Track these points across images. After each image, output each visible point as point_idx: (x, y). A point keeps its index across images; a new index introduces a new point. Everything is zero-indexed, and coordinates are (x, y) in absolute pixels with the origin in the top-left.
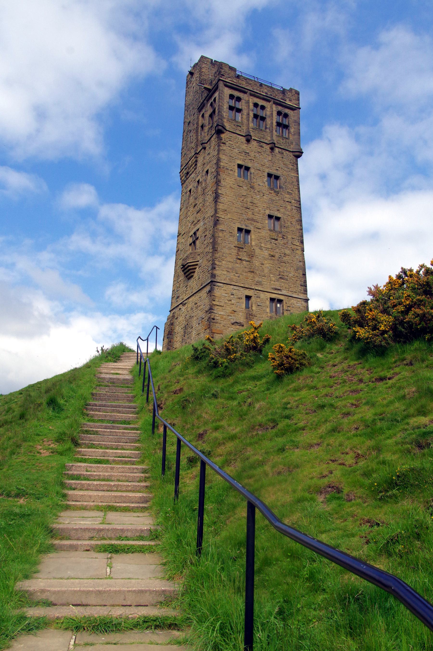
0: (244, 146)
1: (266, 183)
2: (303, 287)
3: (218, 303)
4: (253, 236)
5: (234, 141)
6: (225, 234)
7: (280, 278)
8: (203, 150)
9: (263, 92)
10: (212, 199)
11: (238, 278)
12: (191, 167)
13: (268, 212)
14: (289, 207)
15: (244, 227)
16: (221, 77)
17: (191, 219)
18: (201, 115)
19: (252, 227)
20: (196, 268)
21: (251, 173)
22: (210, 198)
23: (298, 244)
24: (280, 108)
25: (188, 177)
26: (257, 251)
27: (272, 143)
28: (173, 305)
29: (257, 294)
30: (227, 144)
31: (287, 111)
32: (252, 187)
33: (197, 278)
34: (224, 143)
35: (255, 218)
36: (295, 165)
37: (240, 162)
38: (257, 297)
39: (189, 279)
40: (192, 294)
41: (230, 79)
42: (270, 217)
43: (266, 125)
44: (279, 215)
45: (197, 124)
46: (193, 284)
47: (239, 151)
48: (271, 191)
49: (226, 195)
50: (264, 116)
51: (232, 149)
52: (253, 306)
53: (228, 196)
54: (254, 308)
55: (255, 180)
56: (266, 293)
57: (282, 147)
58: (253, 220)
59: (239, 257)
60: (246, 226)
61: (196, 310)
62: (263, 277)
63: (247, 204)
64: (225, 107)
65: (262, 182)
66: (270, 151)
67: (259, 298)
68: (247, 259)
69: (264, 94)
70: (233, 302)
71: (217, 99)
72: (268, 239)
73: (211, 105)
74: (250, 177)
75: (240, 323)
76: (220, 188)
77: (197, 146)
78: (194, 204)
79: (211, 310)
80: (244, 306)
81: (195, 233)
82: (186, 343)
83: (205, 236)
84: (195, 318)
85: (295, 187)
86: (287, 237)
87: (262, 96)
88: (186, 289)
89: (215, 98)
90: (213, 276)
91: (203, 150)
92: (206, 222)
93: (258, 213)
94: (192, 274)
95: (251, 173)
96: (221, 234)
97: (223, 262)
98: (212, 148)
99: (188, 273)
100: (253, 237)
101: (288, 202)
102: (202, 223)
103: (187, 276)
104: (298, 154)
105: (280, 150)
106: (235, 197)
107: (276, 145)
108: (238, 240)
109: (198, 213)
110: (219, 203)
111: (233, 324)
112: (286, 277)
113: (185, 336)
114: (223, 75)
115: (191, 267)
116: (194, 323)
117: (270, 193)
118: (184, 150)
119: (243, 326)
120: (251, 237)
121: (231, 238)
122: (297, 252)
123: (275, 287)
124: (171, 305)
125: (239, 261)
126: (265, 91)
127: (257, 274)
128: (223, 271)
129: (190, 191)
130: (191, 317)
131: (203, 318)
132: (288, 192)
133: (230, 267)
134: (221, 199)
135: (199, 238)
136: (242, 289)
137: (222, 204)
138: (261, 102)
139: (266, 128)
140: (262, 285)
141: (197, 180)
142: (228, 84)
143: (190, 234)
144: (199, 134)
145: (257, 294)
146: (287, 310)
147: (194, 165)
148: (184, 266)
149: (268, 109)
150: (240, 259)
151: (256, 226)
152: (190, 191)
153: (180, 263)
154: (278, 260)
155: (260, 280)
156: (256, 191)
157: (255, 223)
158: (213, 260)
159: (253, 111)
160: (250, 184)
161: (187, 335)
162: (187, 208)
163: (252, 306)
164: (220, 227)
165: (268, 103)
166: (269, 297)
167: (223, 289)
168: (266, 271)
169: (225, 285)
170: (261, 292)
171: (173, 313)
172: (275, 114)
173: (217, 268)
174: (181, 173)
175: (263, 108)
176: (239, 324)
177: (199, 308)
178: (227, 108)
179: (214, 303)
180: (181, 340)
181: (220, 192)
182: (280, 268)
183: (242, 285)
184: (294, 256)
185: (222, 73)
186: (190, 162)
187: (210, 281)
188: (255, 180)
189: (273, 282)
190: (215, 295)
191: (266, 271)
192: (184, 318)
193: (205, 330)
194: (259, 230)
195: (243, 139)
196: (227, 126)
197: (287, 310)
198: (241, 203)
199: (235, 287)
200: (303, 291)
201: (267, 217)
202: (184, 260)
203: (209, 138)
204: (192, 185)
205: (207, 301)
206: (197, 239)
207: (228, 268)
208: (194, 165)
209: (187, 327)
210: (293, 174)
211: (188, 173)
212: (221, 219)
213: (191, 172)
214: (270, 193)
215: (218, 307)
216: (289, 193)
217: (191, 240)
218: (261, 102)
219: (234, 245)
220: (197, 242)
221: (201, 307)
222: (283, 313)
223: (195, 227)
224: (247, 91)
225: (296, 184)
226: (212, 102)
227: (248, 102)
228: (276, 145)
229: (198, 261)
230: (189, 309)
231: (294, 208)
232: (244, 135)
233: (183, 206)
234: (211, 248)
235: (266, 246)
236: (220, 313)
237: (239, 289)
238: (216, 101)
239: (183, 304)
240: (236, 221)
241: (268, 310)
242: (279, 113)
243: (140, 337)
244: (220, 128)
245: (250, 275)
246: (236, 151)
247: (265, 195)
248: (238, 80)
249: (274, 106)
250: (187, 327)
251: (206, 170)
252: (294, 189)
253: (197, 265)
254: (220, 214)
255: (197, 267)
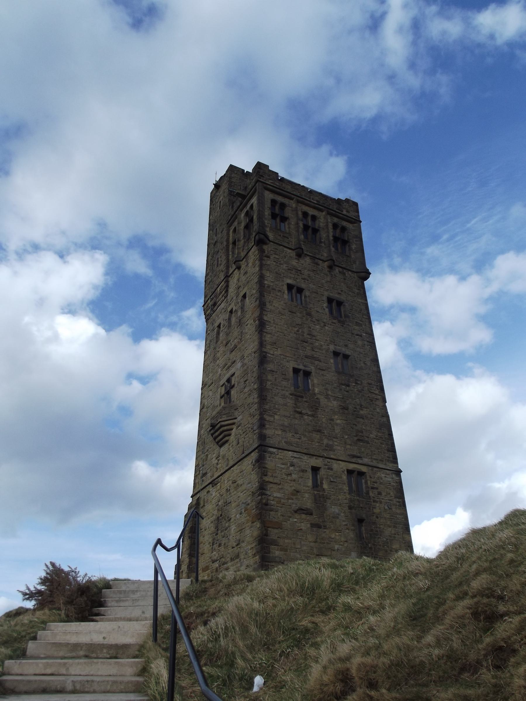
0: (294, 262)
1: (327, 310)
2: (391, 453)
3: (271, 480)
4: (314, 380)
5: (281, 255)
6: (277, 376)
7: (358, 440)
8: (237, 270)
9: (313, 199)
10: (254, 329)
11: (298, 440)
12: (220, 294)
13: (332, 348)
14: (360, 343)
15: (301, 367)
16: (260, 178)
17: (221, 362)
18: (231, 231)
19: (313, 368)
20: (232, 429)
21: (305, 297)
22: (250, 327)
23: (377, 392)
24: (336, 220)
25: (215, 308)
26: (323, 401)
27: (331, 260)
28: (197, 486)
29: (328, 464)
30: (272, 257)
31: (344, 223)
32: (309, 314)
33: (235, 443)
34: (268, 257)
35: (315, 356)
36: (361, 289)
37: (289, 281)
38: (329, 469)
39: (221, 446)
40: (227, 468)
41: (270, 181)
42: (336, 354)
43: (320, 238)
44: (348, 352)
45: (228, 241)
46: (229, 451)
47: (287, 268)
48: (334, 321)
49: (274, 323)
50: (317, 228)
51: (278, 264)
52: (324, 482)
53: (277, 324)
54: (325, 486)
55: (311, 306)
56: (340, 462)
57: (342, 266)
58: (313, 358)
59: (297, 409)
60: (305, 366)
61: (235, 492)
62: (334, 440)
63: (303, 335)
64: (266, 213)
65: (321, 309)
66: (329, 270)
67: (332, 469)
68: (310, 413)
69: (316, 202)
70: (294, 476)
71: (255, 208)
72: (336, 385)
73: (247, 214)
74: (306, 301)
75: (307, 509)
76: (264, 313)
77: (228, 267)
78: (224, 342)
79: (262, 488)
80: (310, 483)
81: (229, 381)
82: (220, 545)
83: (246, 381)
84: (234, 505)
85: (364, 317)
86: (362, 383)
87: (312, 204)
88: (216, 461)
89: (252, 206)
90: (262, 437)
91: (237, 270)
92: (246, 361)
93: (320, 349)
94: (227, 438)
95: (305, 297)
96: (270, 377)
97: (276, 417)
98: (250, 264)
99: (217, 434)
100: (315, 381)
101: (357, 335)
102: (239, 365)
103: (217, 443)
104: (367, 275)
105: (341, 269)
106: (286, 326)
107: (335, 264)
108: (296, 386)
109: (232, 352)
110: (265, 334)
111: (296, 512)
112: (366, 439)
113: (217, 534)
114: (262, 176)
115: (225, 428)
116: (233, 512)
117: (332, 323)
118: (208, 277)
119: (311, 514)
120: (312, 381)
121: (284, 383)
122: (377, 403)
123: (352, 453)
124: (194, 487)
125: (297, 415)
126: (317, 198)
127: (326, 434)
128: (277, 429)
129: (219, 326)
130: (227, 504)
131: (248, 504)
132: (356, 322)
133: (286, 424)
134: (268, 328)
135: (236, 385)
136: (305, 457)
137: (269, 336)
138: (311, 212)
139: (321, 242)
140: (334, 451)
141: (229, 309)
142: (268, 186)
143: (221, 383)
144: (231, 253)
145: (328, 464)
146: (372, 488)
147: (224, 292)
148: (213, 426)
149: (322, 220)
150: (300, 413)
151: (318, 367)
152: (219, 326)
153: (207, 423)
154: (353, 414)
155: (331, 443)
156: (314, 320)
157: (317, 362)
158: (261, 414)
159: (302, 221)
160: (306, 310)
161: (221, 532)
162: (215, 348)
163: (322, 483)
164: (270, 367)
165: (320, 213)
166: (345, 468)
167: (277, 456)
168: (338, 430)
169: (280, 451)
170: (332, 461)
171: (198, 499)
172: (330, 226)
173: (267, 426)
174: (205, 307)
175: (314, 218)
176: (305, 512)
177: (240, 489)
178: (269, 215)
179: (266, 479)
180: (211, 540)
181: (265, 318)
182: (356, 425)
183: (305, 451)
184: (374, 409)
185: (261, 174)
186: (218, 289)
187: (256, 445)
188: (311, 306)
189: (348, 447)
190: (267, 466)
191: (338, 430)
192: (214, 506)
193: (253, 523)
194: (322, 372)
195: (293, 254)
196: (271, 236)
197: (372, 488)
198: (295, 335)
199: (295, 455)
200: (391, 459)
201: (332, 354)
202: (213, 418)
203: (245, 253)
204: (221, 318)
205: (254, 477)
206: (232, 387)
207: (283, 425)
208: (224, 292)
209: (221, 520)
210: (360, 300)
211: (215, 304)
212: (269, 355)
213: (220, 302)
214: (332, 323)
215: (271, 485)
216: (357, 324)
217: (223, 390)
218: (311, 212)
219: (290, 392)
220: (233, 392)
221: (244, 487)
222: (368, 493)
223: (228, 372)
224: (293, 196)
225: (365, 312)
226: (247, 211)
227: (296, 210)
228: (335, 264)
229: (236, 418)
230: (224, 491)
231: (366, 343)
232: (293, 248)
233: (209, 347)
234: (256, 396)
235: (333, 395)
236: (275, 495)
237: (302, 457)
238: (254, 207)
239: (213, 483)
240: (290, 359)
241: (346, 488)
242: (335, 226)
243: (159, 542)
244: (262, 236)
245: (316, 436)
246: (284, 266)
247: (327, 325)
248: (281, 183)
249: (329, 216)
250: (221, 520)
251: (242, 294)
252: (364, 320)
253: (234, 424)
254: (268, 348)
255: (234, 427)
